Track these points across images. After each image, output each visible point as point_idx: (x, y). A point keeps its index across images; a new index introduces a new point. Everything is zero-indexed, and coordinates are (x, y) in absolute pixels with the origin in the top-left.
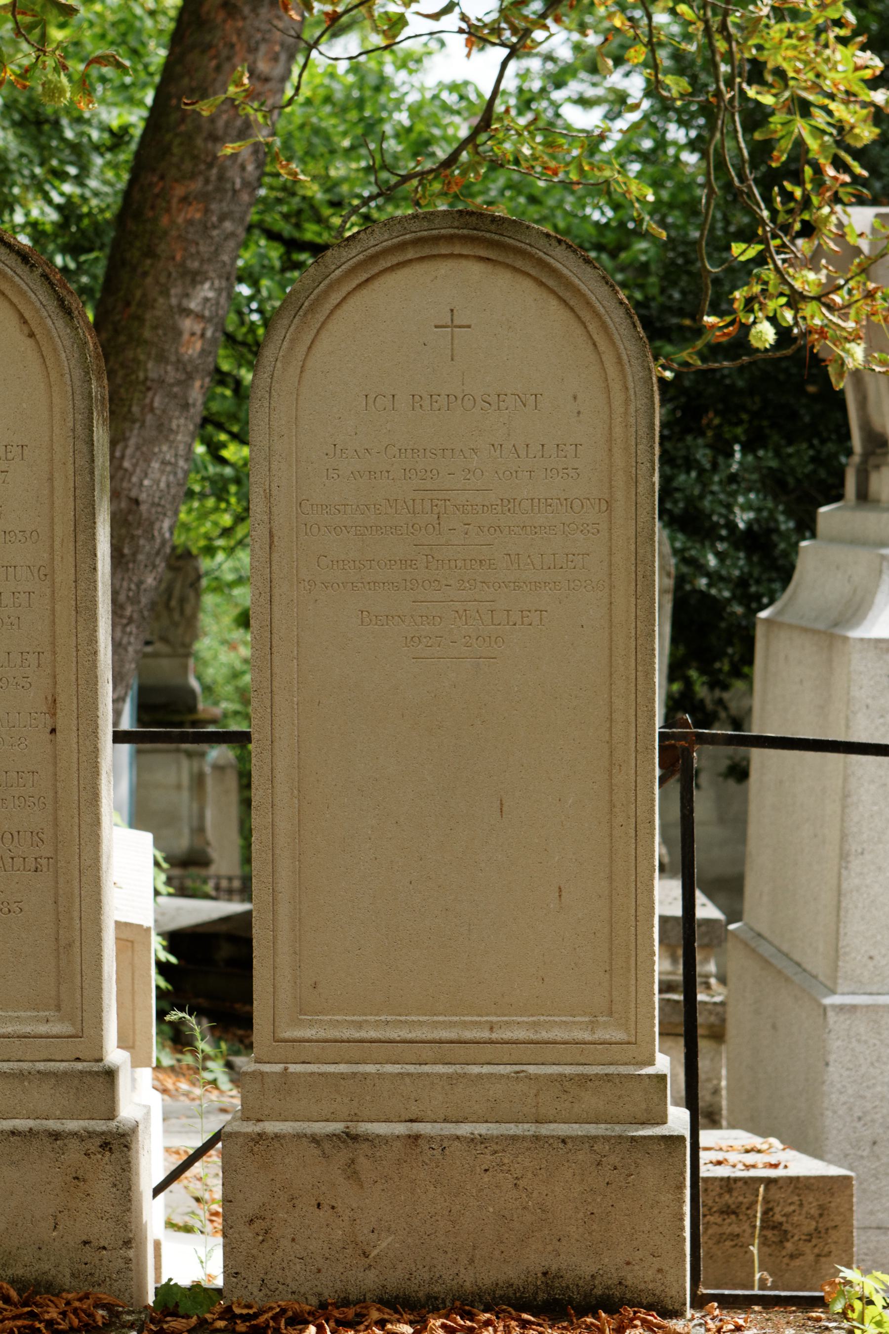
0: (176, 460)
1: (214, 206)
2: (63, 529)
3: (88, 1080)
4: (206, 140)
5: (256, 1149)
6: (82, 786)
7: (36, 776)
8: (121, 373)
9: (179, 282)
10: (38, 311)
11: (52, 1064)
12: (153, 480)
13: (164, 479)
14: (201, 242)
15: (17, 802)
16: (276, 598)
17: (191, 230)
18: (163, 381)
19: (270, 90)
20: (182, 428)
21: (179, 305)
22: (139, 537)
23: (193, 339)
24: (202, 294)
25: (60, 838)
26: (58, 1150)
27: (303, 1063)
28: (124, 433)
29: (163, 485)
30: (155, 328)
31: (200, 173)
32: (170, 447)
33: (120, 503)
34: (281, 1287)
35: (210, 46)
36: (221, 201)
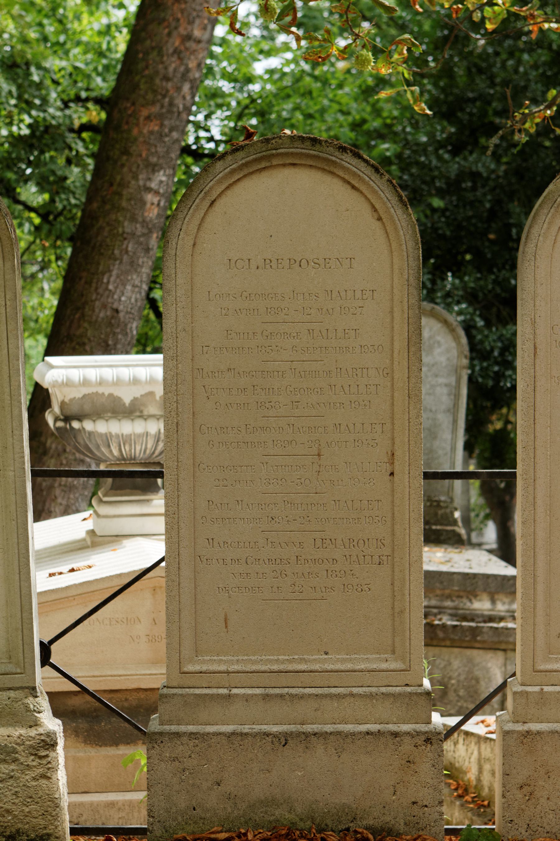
0: (141, 284)
1: (166, 122)
2: (400, 344)
3: (414, 698)
4: (162, 80)
5: (525, 741)
6: (411, 509)
7: (380, 503)
8: (107, 229)
9: (145, 171)
10: (384, 203)
11: (391, 688)
12: (127, 297)
13: (134, 296)
14: (158, 145)
15: (368, 520)
16: (538, 389)
17: (152, 137)
18: (134, 234)
19: (201, 49)
20: (145, 264)
21: (144, 185)
22: (118, 333)
23: (153, 207)
24: (159, 179)
25: (396, 543)
26: (397, 744)
27: (552, 685)
28: (109, 267)
29: (133, 300)
30: (129, 200)
31: (158, 101)
32: (138, 276)
33: (106, 312)
34: (540, 829)
35: (164, 20)
36: (171, 119)
